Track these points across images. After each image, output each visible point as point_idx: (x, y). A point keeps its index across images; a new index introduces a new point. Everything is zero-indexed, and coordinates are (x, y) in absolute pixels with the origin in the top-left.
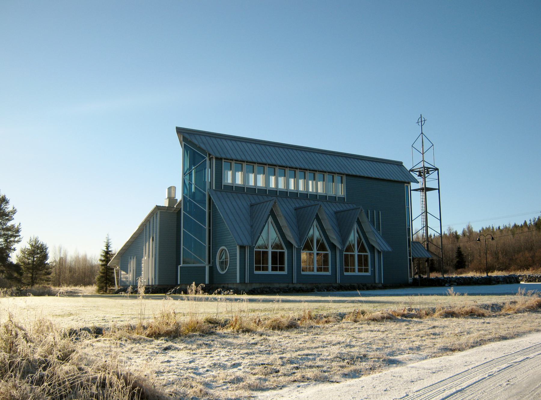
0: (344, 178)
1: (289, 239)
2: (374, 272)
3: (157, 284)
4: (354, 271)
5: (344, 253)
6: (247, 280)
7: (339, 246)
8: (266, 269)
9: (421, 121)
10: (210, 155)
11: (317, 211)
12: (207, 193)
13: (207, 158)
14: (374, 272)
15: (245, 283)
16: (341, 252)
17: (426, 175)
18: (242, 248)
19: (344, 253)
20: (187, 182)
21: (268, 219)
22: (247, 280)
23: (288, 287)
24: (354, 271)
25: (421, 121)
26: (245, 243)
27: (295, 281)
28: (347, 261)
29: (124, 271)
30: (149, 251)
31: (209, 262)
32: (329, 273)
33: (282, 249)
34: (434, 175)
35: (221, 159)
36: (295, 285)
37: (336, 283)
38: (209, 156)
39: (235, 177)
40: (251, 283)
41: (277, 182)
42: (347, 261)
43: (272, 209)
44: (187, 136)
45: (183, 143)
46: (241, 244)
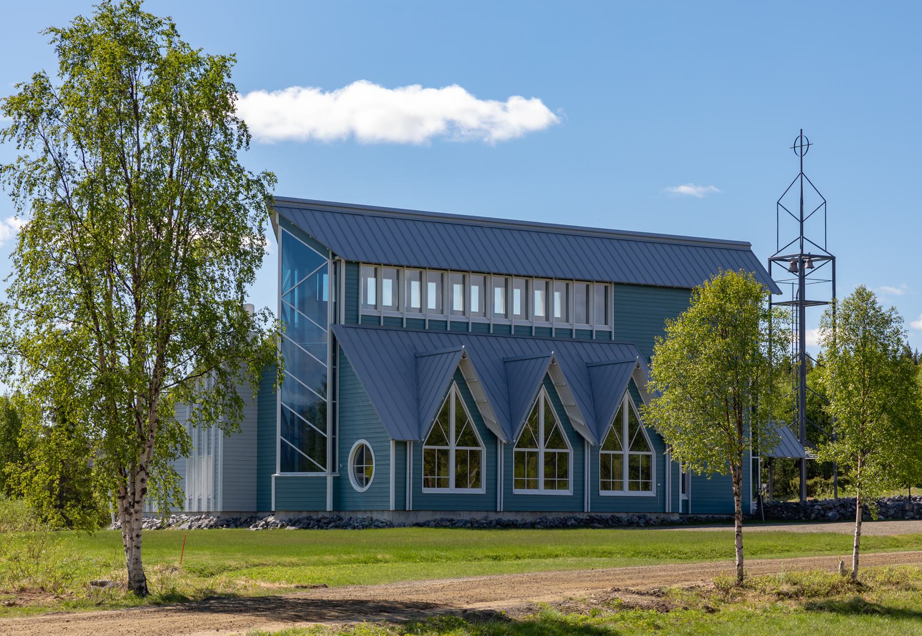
0: (612, 290)
1: (489, 426)
2: (662, 490)
3: (219, 509)
4: (621, 488)
5: (601, 452)
6: (409, 506)
7: (589, 439)
8: (441, 483)
9: (801, 146)
10: (334, 255)
11: (547, 370)
12: (328, 332)
13: (329, 262)
14: (662, 490)
15: (405, 510)
16: (594, 449)
17: (807, 271)
18: (401, 445)
19: (424, 447)
20: (288, 304)
21: (451, 384)
22: (409, 506)
23: (486, 518)
24: (621, 488)
25: (801, 146)
26: (408, 436)
27: (500, 507)
28: (607, 469)
29: (796, 504)
30: (216, 443)
31: (334, 470)
32: (568, 492)
33: (477, 445)
34: (825, 271)
35: (358, 264)
36: (500, 516)
37: (583, 511)
38: (333, 258)
39: (379, 293)
40: (416, 509)
41: (465, 300)
42: (607, 469)
43: (458, 369)
44: (287, 214)
45: (280, 228)
46: (400, 438)
